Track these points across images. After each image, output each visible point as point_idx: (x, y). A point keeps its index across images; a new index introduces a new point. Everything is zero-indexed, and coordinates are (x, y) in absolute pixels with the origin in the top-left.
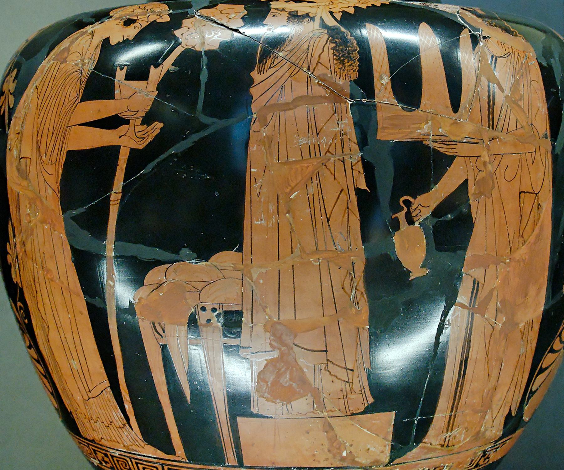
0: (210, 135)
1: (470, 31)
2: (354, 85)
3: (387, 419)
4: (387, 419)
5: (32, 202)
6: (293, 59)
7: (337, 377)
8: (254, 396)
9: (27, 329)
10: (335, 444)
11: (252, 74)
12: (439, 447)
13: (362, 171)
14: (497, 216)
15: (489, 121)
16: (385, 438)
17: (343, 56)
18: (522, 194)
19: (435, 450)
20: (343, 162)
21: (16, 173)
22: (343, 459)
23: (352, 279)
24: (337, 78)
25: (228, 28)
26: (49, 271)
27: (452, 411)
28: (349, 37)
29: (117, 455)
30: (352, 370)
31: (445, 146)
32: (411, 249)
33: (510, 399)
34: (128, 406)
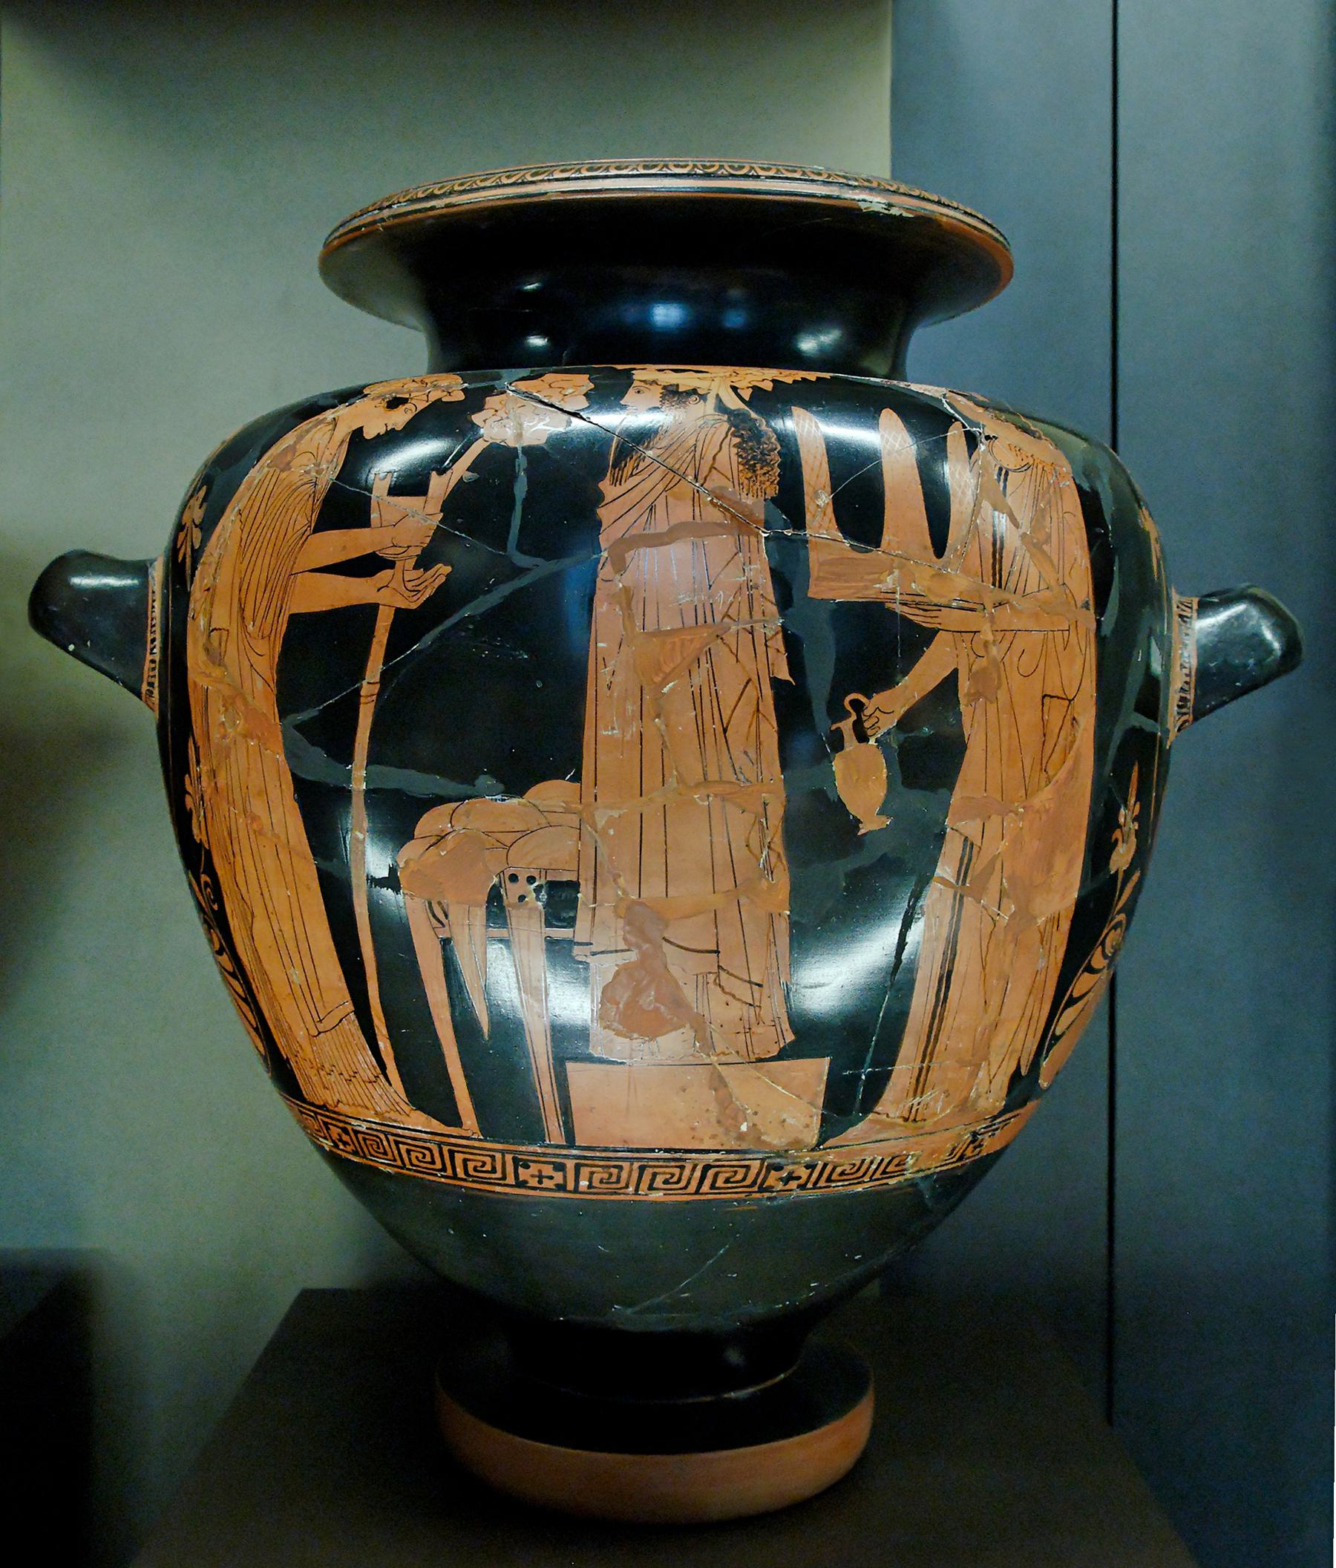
0: (531, 585)
1: (964, 427)
2: (772, 506)
3: (816, 1070)
4: (816, 1070)
5: (228, 704)
6: (671, 462)
7: (734, 996)
8: (596, 1030)
9: (216, 920)
10: (729, 1111)
11: (601, 485)
12: (901, 1121)
13: (782, 649)
14: (1005, 734)
15: (994, 575)
16: (812, 1104)
17: (753, 458)
18: (1047, 699)
19: (893, 1126)
20: (752, 633)
21: (202, 656)
22: (741, 1137)
23: (762, 830)
24: (744, 495)
25: (561, 410)
26: (254, 818)
27: (923, 1061)
28: (764, 427)
29: (364, 1129)
30: (760, 985)
31: (921, 612)
32: (862, 781)
33: (1018, 1045)
34: (384, 1044)
